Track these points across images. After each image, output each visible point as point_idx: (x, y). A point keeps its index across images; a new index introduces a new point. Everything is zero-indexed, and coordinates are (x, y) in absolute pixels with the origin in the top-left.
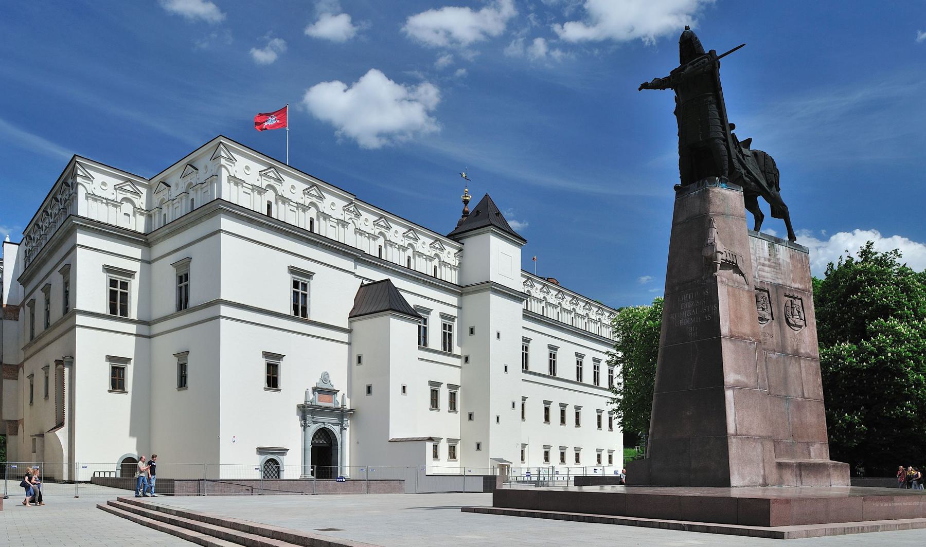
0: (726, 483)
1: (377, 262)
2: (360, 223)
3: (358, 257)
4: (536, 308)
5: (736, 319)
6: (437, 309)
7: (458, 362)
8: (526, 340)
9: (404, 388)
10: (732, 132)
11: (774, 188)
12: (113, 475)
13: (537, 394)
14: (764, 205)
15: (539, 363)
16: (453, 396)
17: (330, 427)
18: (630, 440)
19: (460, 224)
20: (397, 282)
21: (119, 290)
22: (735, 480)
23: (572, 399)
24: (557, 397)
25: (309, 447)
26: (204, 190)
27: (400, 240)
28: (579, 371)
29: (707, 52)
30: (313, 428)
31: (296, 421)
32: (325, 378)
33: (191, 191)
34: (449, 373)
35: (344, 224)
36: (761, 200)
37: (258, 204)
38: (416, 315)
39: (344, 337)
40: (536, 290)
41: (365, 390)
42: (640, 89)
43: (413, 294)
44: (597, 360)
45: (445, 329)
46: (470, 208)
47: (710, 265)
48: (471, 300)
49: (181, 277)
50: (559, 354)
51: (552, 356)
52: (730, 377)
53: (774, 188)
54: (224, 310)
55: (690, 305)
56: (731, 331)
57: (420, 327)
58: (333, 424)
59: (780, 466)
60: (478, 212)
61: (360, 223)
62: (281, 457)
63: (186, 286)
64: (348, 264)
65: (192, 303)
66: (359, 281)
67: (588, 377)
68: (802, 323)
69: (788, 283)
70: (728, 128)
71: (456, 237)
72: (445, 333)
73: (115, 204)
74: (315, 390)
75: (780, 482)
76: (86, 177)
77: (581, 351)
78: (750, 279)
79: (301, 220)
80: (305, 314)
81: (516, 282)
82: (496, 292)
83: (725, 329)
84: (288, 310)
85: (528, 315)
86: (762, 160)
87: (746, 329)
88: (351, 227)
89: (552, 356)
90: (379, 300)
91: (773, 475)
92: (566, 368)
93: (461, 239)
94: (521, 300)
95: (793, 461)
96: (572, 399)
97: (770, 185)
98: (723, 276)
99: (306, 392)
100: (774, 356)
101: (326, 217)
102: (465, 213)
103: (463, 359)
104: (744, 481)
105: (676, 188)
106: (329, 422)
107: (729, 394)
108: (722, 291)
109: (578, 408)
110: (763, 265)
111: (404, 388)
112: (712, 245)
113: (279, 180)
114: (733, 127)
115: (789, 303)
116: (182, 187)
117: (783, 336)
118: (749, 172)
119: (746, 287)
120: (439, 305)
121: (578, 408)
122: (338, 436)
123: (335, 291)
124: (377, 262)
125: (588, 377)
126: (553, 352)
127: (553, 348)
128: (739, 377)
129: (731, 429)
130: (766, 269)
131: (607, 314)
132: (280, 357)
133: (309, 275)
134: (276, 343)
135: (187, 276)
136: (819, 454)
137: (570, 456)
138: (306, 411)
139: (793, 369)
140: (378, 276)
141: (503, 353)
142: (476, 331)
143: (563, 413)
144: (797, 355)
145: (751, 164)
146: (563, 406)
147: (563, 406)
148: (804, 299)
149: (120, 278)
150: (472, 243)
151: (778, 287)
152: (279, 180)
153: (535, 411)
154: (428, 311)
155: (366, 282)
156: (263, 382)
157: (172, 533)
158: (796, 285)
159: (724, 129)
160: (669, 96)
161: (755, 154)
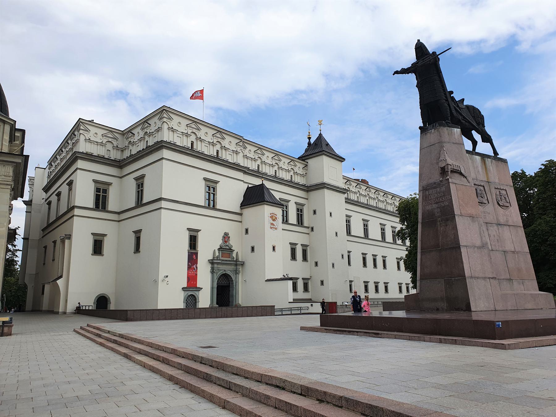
1: (257, 173)
2: (246, 152)
3: (246, 171)
4: (353, 197)
6: (293, 200)
9: (274, 247)
10: (452, 95)
11: (481, 126)
12: (91, 308)
13: (357, 250)
14: (477, 137)
15: (357, 229)
17: (229, 273)
19: (306, 150)
21: (101, 194)
24: (370, 251)
25: (215, 285)
26: (154, 136)
27: (269, 161)
29: (431, 53)
33: (146, 137)
34: (299, 238)
35: (237, 153)
36: (474, 132)
37: (186, 142)
38: (282, 204)
41: (250, 249)
42: (394, 74)
43: (278, 191)
46: (312, 141)
49: (139, 185)
53: (481, 126)
57: (283, 211)
61: (246, 152)
62: (197, 293)
63: (142, 190)
65: (145, 201)
68: (508, 205)
70: (448, 94)
72: (298, 214)
78: (470, 180)
79: (211, 151)
82: (328, 188)
85: (348, 201)
88: (241, 155)
89: (348, 221)
90: (255, 197)
92: (375, 232)
94: (345, 193)
96: (380, 252)
97: (478, 124)
101: (226, 149)
102: (309, 144)
103: (310, 229)
105: (420, 128)
111: (274, 247)
114: (452, 92)
115: (498, 193)
116: (142, 134)
118: (464, 117)
120: (294, 197)
124: (257, 173)
126: (366, 223)
133: (216, 182)
134: (195, 222)
137: (381, 287)
140: (257, 182)
142: (317, 212)
143: (375, 260)
145: (465, 113)
146: (374, 256)
150: (312, 162)
152: (199, 129)
153: (357, 260)
154: (288, 201)
155: (250, 186)
157: (112, 349)
159: (445, 94)
160: (412, 78)
161: (468, 107)
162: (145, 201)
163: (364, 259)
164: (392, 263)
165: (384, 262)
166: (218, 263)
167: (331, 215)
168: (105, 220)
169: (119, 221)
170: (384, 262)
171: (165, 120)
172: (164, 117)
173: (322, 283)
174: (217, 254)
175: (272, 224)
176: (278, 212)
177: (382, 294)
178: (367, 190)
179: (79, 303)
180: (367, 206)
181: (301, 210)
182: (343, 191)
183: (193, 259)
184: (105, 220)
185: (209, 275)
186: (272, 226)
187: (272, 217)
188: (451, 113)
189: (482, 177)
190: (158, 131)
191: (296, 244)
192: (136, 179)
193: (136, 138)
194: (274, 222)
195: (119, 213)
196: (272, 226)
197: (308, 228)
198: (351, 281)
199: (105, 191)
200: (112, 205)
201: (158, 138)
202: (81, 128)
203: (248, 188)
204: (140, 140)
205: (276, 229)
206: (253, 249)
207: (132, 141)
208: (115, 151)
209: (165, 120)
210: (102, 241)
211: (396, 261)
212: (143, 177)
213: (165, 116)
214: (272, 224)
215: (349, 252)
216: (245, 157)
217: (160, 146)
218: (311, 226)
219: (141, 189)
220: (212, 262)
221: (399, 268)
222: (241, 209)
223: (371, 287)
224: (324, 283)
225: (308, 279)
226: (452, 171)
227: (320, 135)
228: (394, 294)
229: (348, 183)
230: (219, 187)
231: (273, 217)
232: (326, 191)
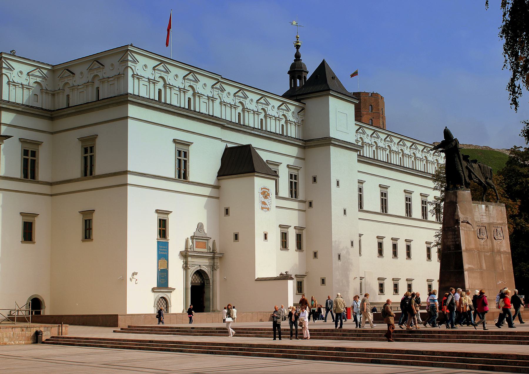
4: (368, 152)
8: (361, 182)
13: (371, 230)
21: (30, 158)
24: (389, 232)
28: (409, 208)
30: (192, 270)
39: (207, 191)
43: (266, 150)
45: (291, 178)
47: (457, 222)
48: (315, 152)
50: (390, 192)
51: (384, 195)
52: (466, 266)
55: (451, 237)
56: (466, 248)
62: (168, 294)
63: (91, 157)
65: (98, 171)
67: (417, 212)
69: (495, 221)
72: (25, 161)
76: (9, 69)
77: (409, 188)
80: (185, 177)
81: (351, 137)
83: (463, 247)
84: (172, 173)
85: (362, 159)
86: (482, 168)
87: (473, 246)
89: (384, 195)
92: (396, 205)
99: (187, 241)
100: (488, 254)
103: (307, 204)
107: (466, 273)
108: (462, 233)
110: (483, 215)
111: (265, 235)
112: (458, 216)
113: (167, 72)
117: (492, 243)
119: (473, 230)
122: (210, 277)
124: (238, 127)
125: (417, 212)
128: (470, 266)
130: (484, 217)
132: (167, 213)
134: (165, 201)
135: (92, 149)
139: (498, 258)
140: (243, 140)
141: (342, 197)
143: (395, 246)
144: (499, 252)
148: (503, 227)
151: (489, 224)
154: (277, 164)
155: (230, 145)
158: (500, 222)
163: (380, 245)
164: (419, 250)
165: (408, 248)
166: (193, 256)
168: (36, 193)
169: (51, 195)
170: (408, 248)
173: (323, 281)
175: (264, 203)
176: (270, 184)
178: (388, 139)
180: (387, 165)
183: (163, 253)
184: (36, 193)
185: (181, 272)
186: (263, 206)
187: (263, 193)
188: (465, 179)
189: (485, 220)
190: (118, 78)
191: (288, 227)
192: (82, 140)
193: (78, 80)
194: (266, 201)
195: (51, 184)
196: (263, 206)
197: (304, 202)
198: (361, 278)
199: (34, 154)
200: (43, 174)
203: (227, 149)
204: (86, 85)
205: (268, 209)
206: (236, 237)
207: (71, 83)
208: (44, 95)
210: (31, 223)
211: (425, 247)
212: (94, 138)
214: (264, 203)
215: (360, 235)
218: (310, 199)
220: (185, 255)
221: (429, 257)
222: (219, 180)
224: (326, 281)
225: (303, 276)
226: (462, 222)
229: (360, 131)
230: (192, 150)
231: (265, 194)
232: (332, 148)
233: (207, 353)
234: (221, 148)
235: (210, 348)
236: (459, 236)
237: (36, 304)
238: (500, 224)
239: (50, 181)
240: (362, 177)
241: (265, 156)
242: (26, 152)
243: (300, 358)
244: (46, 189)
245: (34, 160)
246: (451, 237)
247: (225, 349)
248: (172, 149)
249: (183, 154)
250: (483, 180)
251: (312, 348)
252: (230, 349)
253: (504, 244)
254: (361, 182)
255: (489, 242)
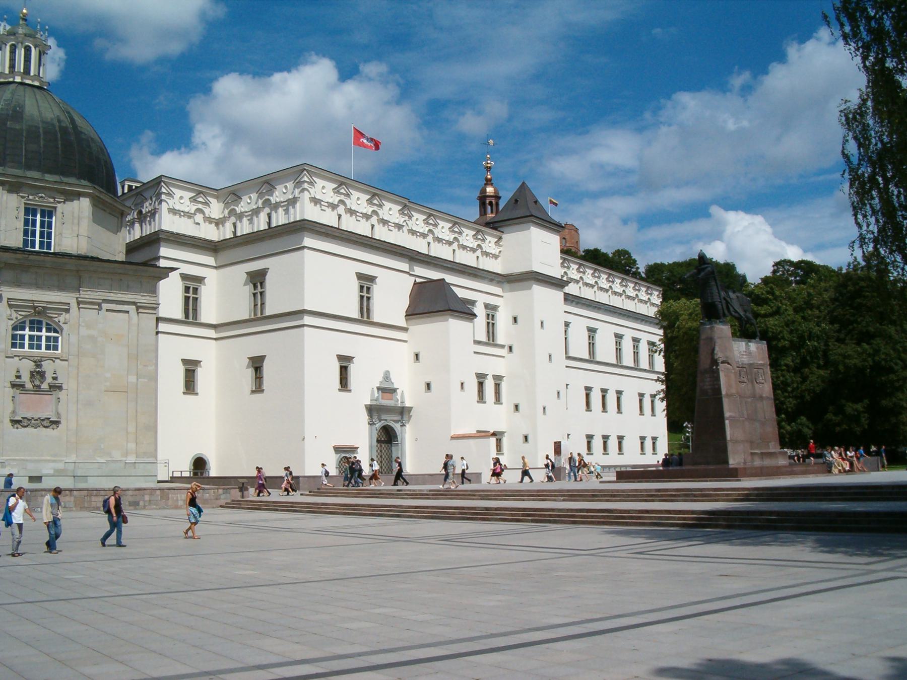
0: (727, 462)
4: (572, 289)
5: (729, 386)
7: (504, 352)
13: (581, 378)
16: (497, 386)
17: (392, 424)
18: (674, 427)
20: (450, 278)
22: (731, 461)
23: (613, 383)
24: (598, 381)
28: (619, 351)
30: (378, 425)
31: (365, 417)
32: (387, 377)
35: (399, 227)
40: (573, 272)
43: (463, 288)
44: (636, 341)
52: (727, 414)
54: (308, 320)
55: (708, 379)
58: (394, 421)
59: (752, 454)
60: (516, 201)
64: (405, 266)
66: (413, 278)
67: (628, 360)
71: (496, 225)
72: (187, 299)
73: (189, 215)
74: (378, 389)
75: (753, 461)
77: (620, 330)
81: (556, 272)
83: (724, 392)
85: (569, 299)
87: (733, 391)
91: (749, 459)
92: (605, 350)
93: (501, 227)
95: (758, 451)
96: (613, 383)
98: (722, 367)
100: (749, 400)
103: (507, 348)
104: (734, 461)
106: (390, 420)
107: (727, 422)
109: (619, 393)
121: (619, 393)
123: (394, 290)
125: (628, 360)
127: (592, 331)
129: (728, 438)
131: (644, 289)
136: (774, 447)
137: (613, 444)
138: (371, 410)
144: (761, 398)
147: (604, 391)
149: (192, 285)
151: (751, 365)
154: (473, 303)
155: (419, 280)
156: (338, 386)
162: (268, 312)
164: (630, 402)
167: (542, 326)
171: (306, 186)
172: (305, 181)
174: (376, 395)
177: (614, 459)
179: (259, 469)
181: (493, 316)
182: (558, 283)
199: (196, 290)
201: (296, 214)
202: (163, 190)
209: (306, 186)
213: (306, 179)
216: (412, 232)
217: (303, 227)
219: (259, 289)
223: (597, 443)
227: (524, 183)
228: (633, 458)
233: (432, 518)
234: (409, 282)
235: (434, 512)
236: (718, 379)
237: (200, 464)
238: (761, 365)
239: (214, 323)
240: (570, 318)
241: (461, 293)
242: (187, 289)
243: (555, 522)
244: (211, 333)
245: (197, 299)
246: (708, 379)
247: (454, 513)
248: (355, 284)
249: (365, 289)
250: (742, 314)
251: (568, 510)
252: (461, 513)
253: (766, 388)
254: (567, 324)
255: (750, 385)
